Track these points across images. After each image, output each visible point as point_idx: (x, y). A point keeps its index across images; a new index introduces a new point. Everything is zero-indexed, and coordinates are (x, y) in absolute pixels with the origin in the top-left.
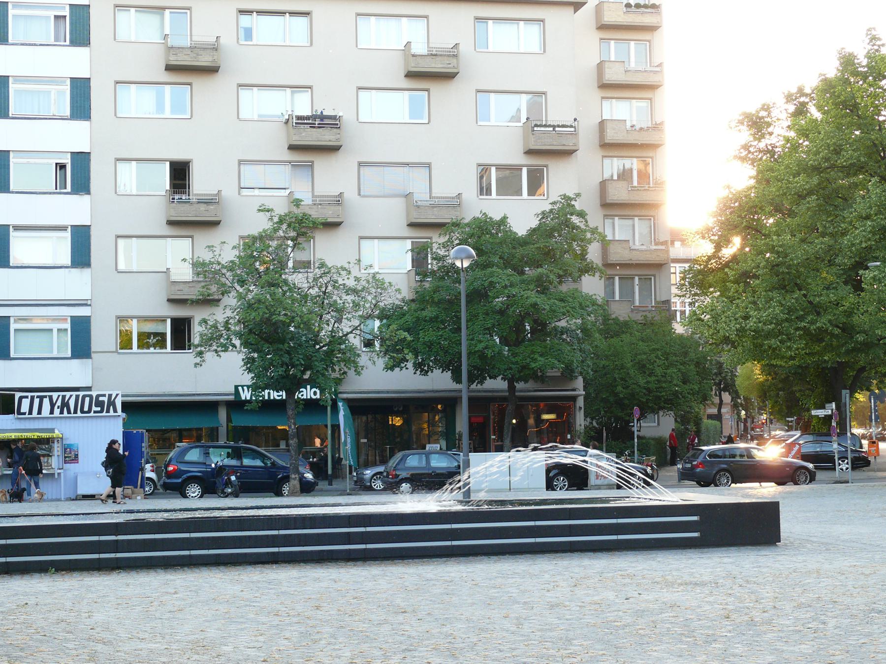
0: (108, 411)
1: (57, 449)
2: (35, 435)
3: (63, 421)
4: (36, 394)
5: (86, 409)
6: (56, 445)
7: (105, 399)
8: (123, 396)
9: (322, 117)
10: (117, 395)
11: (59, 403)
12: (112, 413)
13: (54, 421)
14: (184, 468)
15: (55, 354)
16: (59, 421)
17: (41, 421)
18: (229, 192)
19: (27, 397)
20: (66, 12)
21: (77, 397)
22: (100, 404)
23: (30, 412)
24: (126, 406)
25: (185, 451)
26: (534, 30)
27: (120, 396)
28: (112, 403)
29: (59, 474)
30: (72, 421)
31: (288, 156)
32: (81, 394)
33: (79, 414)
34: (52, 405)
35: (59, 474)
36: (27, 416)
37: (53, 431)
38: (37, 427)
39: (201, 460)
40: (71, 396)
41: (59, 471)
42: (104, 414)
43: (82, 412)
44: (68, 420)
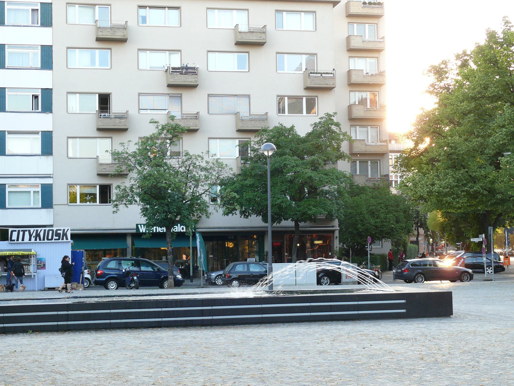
0: (63, 239)
1: (33, 261)
2: (21, 253)
3: (37, 245)
4: (21, 229)
5: (50, 238)
6: (32, 259)
7: (61, 232)
8: (71, 230)
9: (187, 68)
10: (68, 230)
11: (34, 234)
12: (65, 240)
13: (31, 245)
14: (107, 272)
15: (32, 206)
16: (34, 245)
17: (24, 245)
18: (133, 111)
19: (15, 231)
20: (39, 7)
21: (45, 231)
22: (58, 235)
23: (18, 240)
24: (73, 236)
25: (107, 262)
26: (310, 18)
27: (69, 230)
28: (65, 234)
29: (34, 276)
30: (42, 245)
31: (167, 91)
32: (47, 229)
33: (46, 241)
34: (30, 236)
35: (34, 276)
36: (16, 242)
37: (30, 250)
38: (21, 248)
39: (117, 267)
40: (41, 230)
41: (34, 274)
42: (60, 241)
43: (48, 239)
44: (39, 244)
